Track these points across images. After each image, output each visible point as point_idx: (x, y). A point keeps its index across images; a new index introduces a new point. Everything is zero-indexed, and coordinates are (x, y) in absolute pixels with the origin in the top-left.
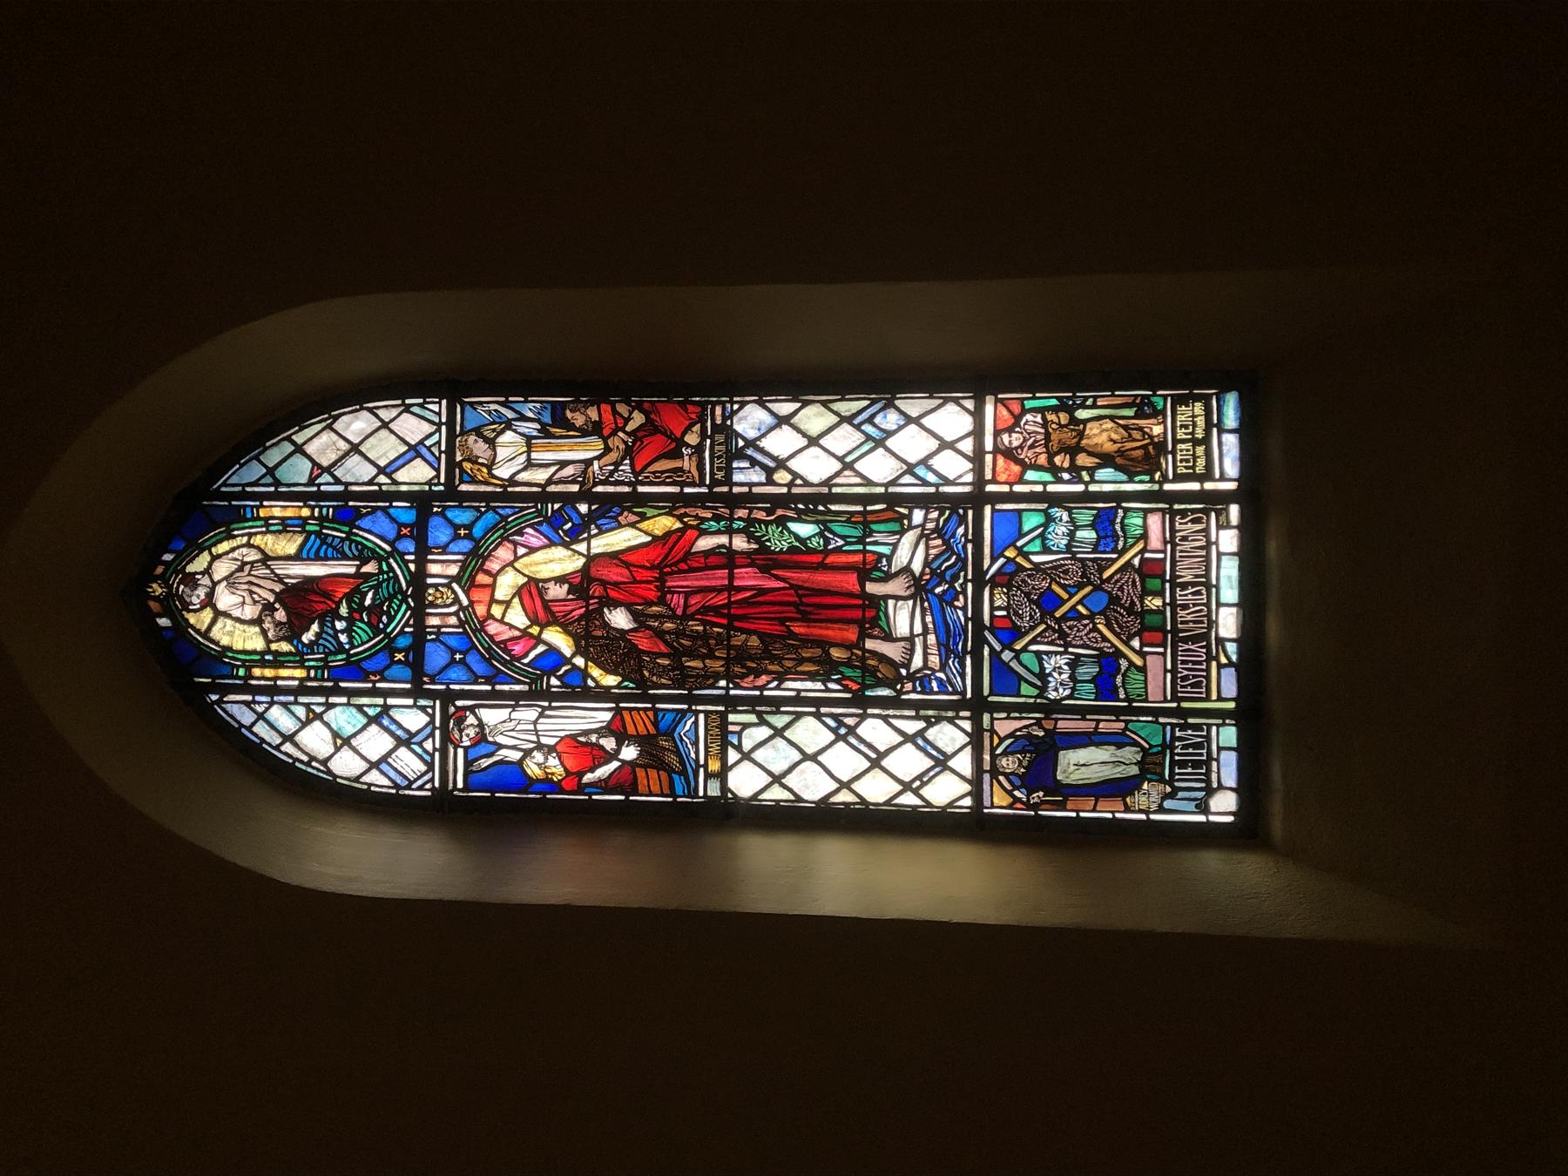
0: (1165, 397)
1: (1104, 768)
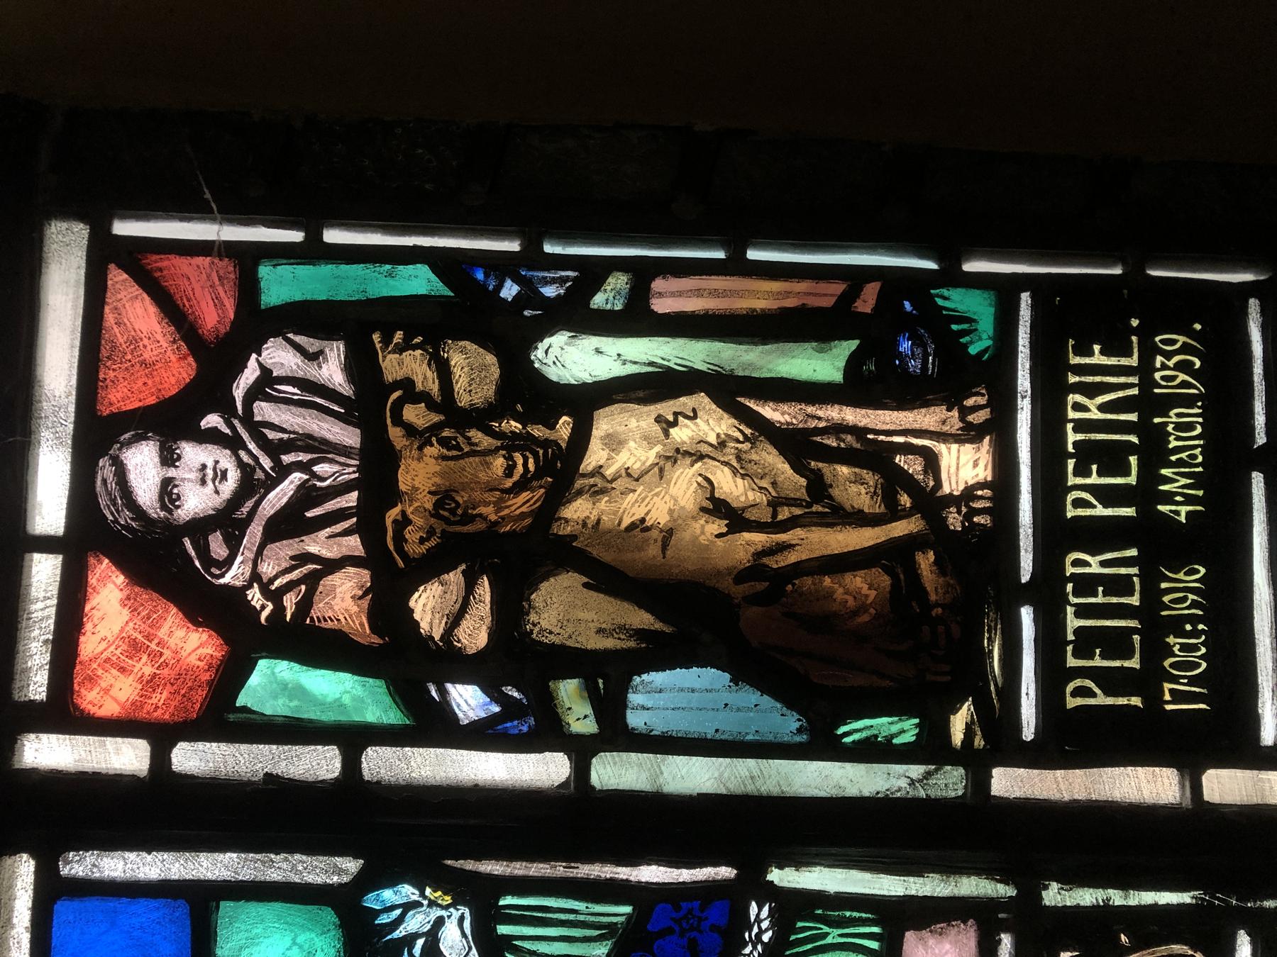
0: (1005, 290)
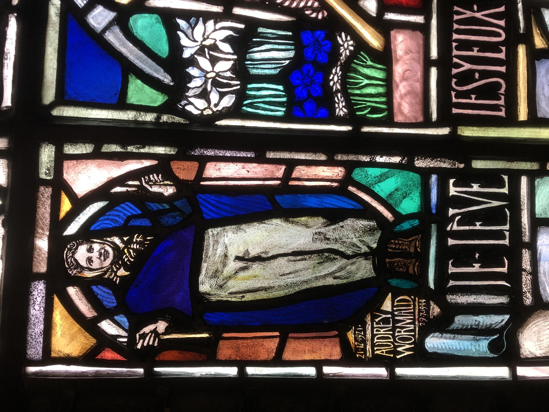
1: (300, 265)
